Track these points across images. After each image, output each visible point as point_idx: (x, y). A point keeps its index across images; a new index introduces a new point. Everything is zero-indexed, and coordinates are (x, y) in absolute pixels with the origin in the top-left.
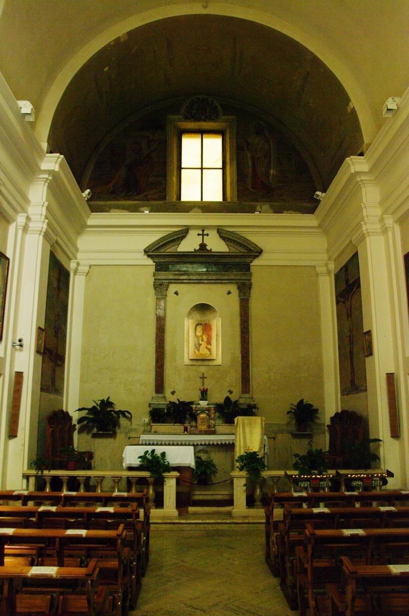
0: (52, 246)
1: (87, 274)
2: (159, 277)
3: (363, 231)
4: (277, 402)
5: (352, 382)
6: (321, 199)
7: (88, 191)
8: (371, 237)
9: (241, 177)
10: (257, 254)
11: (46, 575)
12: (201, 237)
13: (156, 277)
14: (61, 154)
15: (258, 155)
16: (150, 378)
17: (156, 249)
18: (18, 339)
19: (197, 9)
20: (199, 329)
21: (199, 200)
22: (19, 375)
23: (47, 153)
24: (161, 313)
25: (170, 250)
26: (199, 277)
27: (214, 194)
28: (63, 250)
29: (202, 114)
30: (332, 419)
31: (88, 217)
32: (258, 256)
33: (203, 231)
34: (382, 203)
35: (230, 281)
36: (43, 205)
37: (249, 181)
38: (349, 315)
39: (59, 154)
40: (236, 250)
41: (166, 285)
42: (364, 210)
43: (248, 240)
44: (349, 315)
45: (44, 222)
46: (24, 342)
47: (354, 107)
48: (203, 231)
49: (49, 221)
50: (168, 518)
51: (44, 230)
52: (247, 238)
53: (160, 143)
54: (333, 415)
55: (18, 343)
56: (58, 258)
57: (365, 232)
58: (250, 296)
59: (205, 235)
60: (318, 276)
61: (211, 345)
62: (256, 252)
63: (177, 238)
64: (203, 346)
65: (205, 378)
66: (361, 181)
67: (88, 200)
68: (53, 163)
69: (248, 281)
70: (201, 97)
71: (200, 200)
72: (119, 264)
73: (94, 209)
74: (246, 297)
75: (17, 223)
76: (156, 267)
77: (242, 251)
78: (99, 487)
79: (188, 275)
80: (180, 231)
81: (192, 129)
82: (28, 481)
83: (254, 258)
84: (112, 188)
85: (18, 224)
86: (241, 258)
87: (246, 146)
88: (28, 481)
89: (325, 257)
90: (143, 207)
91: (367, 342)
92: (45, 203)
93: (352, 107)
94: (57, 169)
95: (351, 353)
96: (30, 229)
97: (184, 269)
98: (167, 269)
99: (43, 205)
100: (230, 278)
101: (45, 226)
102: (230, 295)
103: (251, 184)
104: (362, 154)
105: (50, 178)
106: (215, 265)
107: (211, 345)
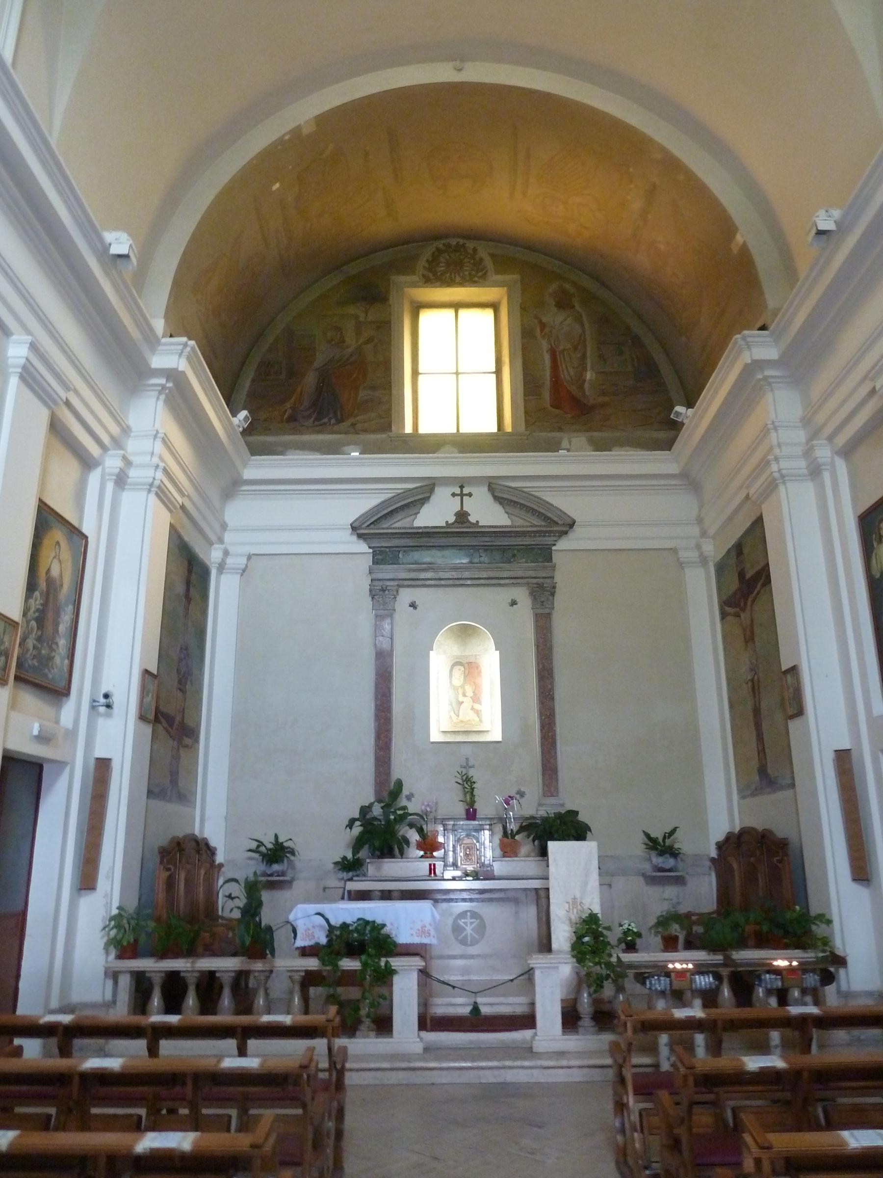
1: (244, 571)
2: (380, 576)
4: (621, 816)
5: (762, 770)
6: (685, 421)
7: (244, 414)
8: (788, 484)
10: (564, 529)
11: (243, 1068)
13: (375, 576)
14: (190, 339)
15: (561, 347)
18: (103, 691)
20: (458, 672)
21: (455, 431)
22: (103, 766)
24: (385, 644)
25: (400, 523)
26: (454, 574)
27: (481, 419)
30: (720, 846)
31: (245, 465)
32: (566, 533)
33: (462, 487)
34: (806, 422)
35: (516, 581)
37: (546, 395)
38: (749, 638)
39: (184, 339)
40: (523, 522)
46: (116, 700)
48: (462, 487)
50: (404, 1057)
55: (103, 701)
59: (466, 495)
60: (683, 568)
61: (480, 704)
66: (766, 378)
67: (246, 432)
69: (548, 581)
70: (453, 242)
73: (256, 450)
74: (547, 611)
75: (103, 470)
78: (261, 993)
79: (433, 570)
80: (416, 488)
82: (116, 982)
83: (560, 536)
84: (289, 412)
85: (107, 470)
86: (535, 536)
87: (538, 330)
88: (116, 982)
89: (695, 531)
90: (348, 444)
91: (791, 690)
95: (757, 711)
96: (129, 480)
98: (395, 561)
99: (155, 437)
104: (763, 328)
106: (486, 550)
107: (480, 704)
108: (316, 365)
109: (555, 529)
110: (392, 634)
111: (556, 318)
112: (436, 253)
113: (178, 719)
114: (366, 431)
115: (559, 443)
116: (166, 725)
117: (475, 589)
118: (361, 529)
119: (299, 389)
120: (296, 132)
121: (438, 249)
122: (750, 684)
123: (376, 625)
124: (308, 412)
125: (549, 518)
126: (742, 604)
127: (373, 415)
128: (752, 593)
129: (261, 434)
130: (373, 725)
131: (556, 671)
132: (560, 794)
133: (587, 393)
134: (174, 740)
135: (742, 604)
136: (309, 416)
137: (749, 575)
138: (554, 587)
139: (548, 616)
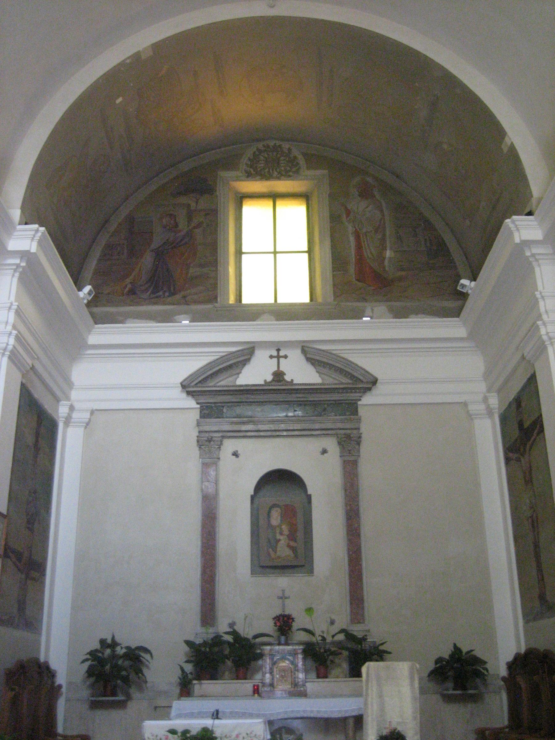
0: (23, 376)
2: (207, 428)
3: (540, 336)
5: (542, 597)
6: (470, 292)
7: (88, 288)
9: (338, 262)
12: (275, 360)
13: (201, 428)
14: (41, 226)
15: (364, 230)
16: (193, 601)
17: (200, 382)
19: (260, 10)
21: (272, 301)
23: (20, 224)
25: (224, 382)
26: (272, 427)
27: (296, 289)
28: (43, 382)
29: (271, 157)
30: (511, 666)
31: (90, 332)
32: (370, 389)
33: (278, 350)
35: (325, 432)
36: (10, 308)
37: (352, 269)
38: (529, 481)
39: (36, 226)
40: (333, 380)
41: (218, 441)
42: (541, 303)
43: (353, 363)
44: (529, 481)
45: (10, 334)
47: (512, 143)
48: (278, 350)
49: (19, 332)
51: (10, 347)
52: (350, 359)
53: (206, 215)
54: (510, 658)
56: (36, 396)
57: (545, 338)
58: (359, 456)
59: (282, 357)
60: (472, 419)
62: (367, 383)
63: (235, 364)
64: (282, 542)
65: (286, 598)
66: (533, 255)
67: (89, 305)
68: (27, 239)
69: (355, 432)
71: (273, 302)
72: (141, 408)
73: (98, 320)
76: (201, 412)
77: (344, 381)
79: (253, 422)
81: (255, 193)
83: (365, 392)
84: (129, 286)
89: (482, 387)
90: (179, 314)
92: (14, 304)
93: (509, 144)
94: (34, 248)
95: (536, 545)
97: (250, 413)
98: (220, 415)
99: (10, 308)
100: (324, 426)
101: (12, 341)
102: (325, 455)
103: (356, 276)
104: (530, 214)
105: (23, 264)
108: (154, 246)
109: (360, 386)
110: (216, 481)
111: (360, 206)
112: (257, 153)
113: (26, 554)
114: (195, 302)
115: (364, 311)
116: (14, 560)
117: (290, 440)
118: (191, 387)
119: (137, 270)
120: (137, 56)
121: (258, 149)
122: (530, 520)
123: (203, 472)
124: (147, 286)
125: (354, 377)
126: (522, 450)
127: (201, 288)
128: (530, 440)
129: (104, 306)
130: (199, 560)
131: (361, 510)
132: (366, 622)
133: (387, 269)
134: (22, 573)
135: (522, 450)
136: (146, 290)
137: (527, 424)
138: (360, 437)
139: (355, 463)
